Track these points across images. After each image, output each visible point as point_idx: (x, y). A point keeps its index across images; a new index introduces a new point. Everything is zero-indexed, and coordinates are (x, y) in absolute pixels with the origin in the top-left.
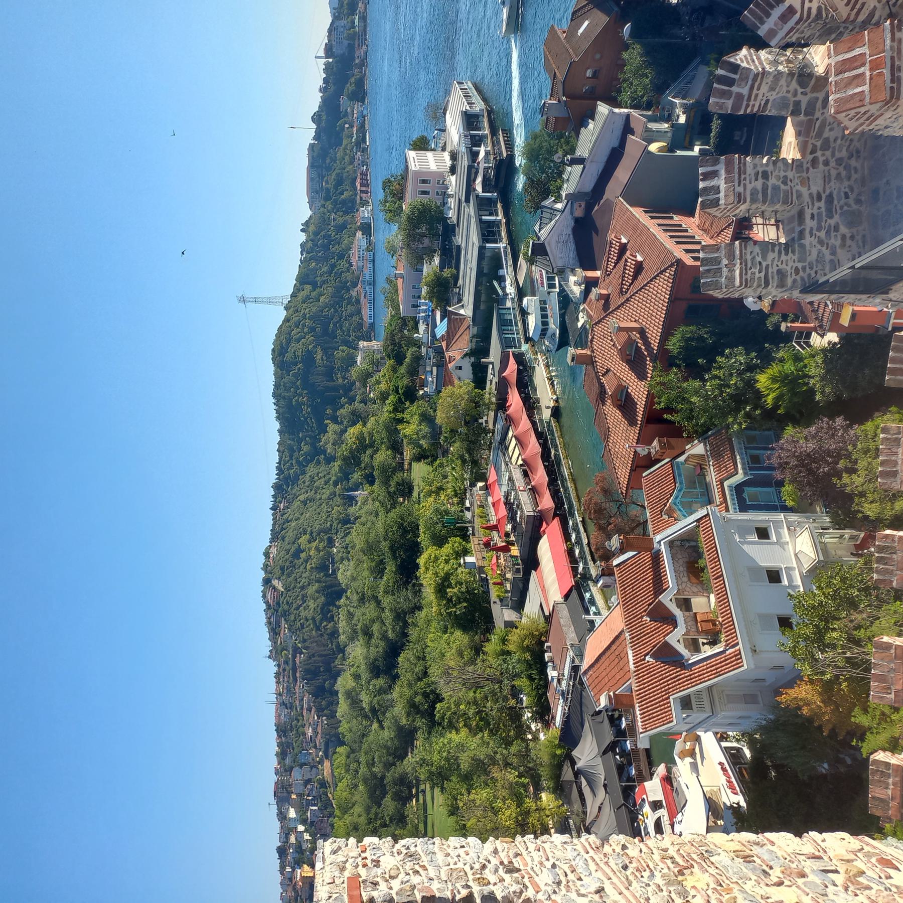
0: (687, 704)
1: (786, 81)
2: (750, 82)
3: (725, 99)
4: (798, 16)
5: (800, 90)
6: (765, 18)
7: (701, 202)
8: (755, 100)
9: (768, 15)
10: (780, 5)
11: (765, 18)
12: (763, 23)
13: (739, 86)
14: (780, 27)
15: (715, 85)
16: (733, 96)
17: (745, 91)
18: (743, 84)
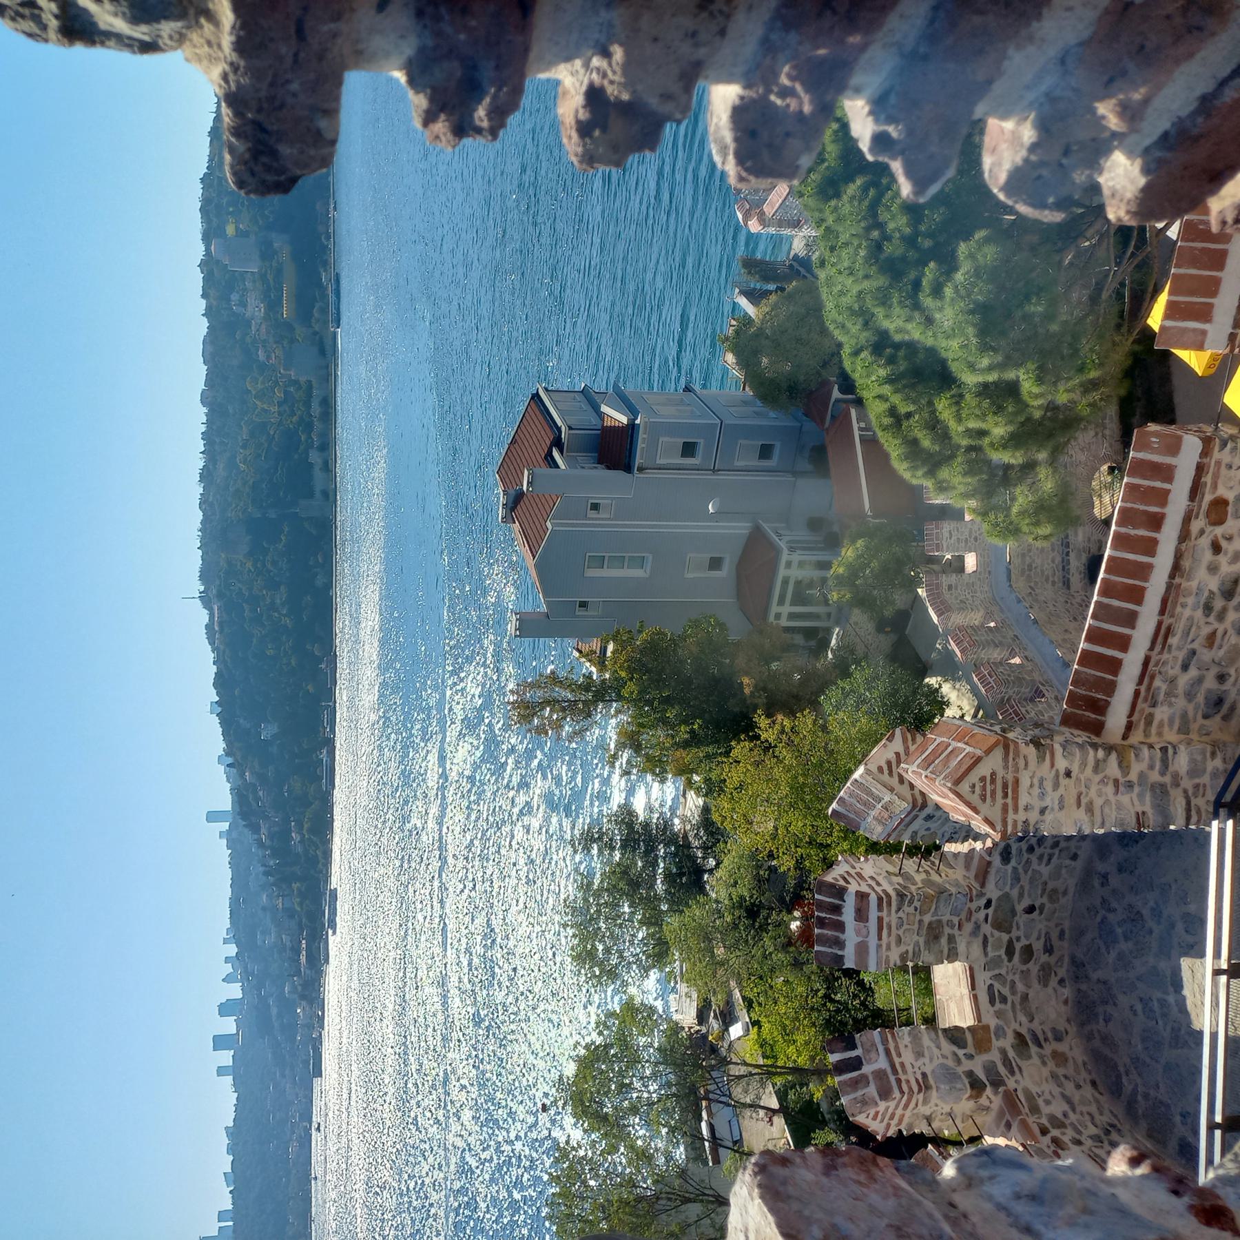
0: (1212, 569)
1: (931, 1040)
2: (881, 1048)
3: (862, 1089)
4: (873, 897)
5: (961, 1052)
6: (841, 935)
7: (739, 113)
8: (904, 1071)
9: (840, 927)
10: (845, 897)
11: (841, 935)
12: (840, 944)
13: (869, 1062)
14: (864, 931)
15: (817, 931)
16: (871, 1078)
17: (882, 1063)
18: (873, 1055)
